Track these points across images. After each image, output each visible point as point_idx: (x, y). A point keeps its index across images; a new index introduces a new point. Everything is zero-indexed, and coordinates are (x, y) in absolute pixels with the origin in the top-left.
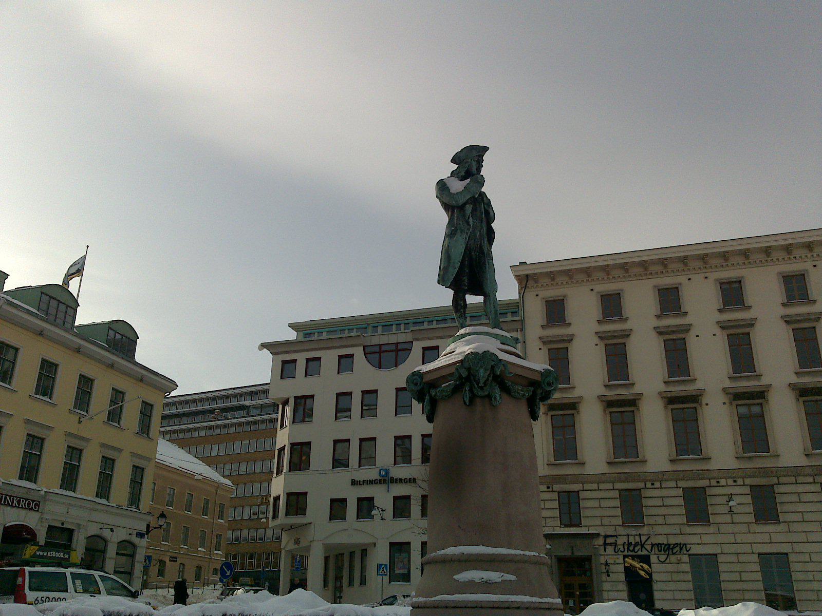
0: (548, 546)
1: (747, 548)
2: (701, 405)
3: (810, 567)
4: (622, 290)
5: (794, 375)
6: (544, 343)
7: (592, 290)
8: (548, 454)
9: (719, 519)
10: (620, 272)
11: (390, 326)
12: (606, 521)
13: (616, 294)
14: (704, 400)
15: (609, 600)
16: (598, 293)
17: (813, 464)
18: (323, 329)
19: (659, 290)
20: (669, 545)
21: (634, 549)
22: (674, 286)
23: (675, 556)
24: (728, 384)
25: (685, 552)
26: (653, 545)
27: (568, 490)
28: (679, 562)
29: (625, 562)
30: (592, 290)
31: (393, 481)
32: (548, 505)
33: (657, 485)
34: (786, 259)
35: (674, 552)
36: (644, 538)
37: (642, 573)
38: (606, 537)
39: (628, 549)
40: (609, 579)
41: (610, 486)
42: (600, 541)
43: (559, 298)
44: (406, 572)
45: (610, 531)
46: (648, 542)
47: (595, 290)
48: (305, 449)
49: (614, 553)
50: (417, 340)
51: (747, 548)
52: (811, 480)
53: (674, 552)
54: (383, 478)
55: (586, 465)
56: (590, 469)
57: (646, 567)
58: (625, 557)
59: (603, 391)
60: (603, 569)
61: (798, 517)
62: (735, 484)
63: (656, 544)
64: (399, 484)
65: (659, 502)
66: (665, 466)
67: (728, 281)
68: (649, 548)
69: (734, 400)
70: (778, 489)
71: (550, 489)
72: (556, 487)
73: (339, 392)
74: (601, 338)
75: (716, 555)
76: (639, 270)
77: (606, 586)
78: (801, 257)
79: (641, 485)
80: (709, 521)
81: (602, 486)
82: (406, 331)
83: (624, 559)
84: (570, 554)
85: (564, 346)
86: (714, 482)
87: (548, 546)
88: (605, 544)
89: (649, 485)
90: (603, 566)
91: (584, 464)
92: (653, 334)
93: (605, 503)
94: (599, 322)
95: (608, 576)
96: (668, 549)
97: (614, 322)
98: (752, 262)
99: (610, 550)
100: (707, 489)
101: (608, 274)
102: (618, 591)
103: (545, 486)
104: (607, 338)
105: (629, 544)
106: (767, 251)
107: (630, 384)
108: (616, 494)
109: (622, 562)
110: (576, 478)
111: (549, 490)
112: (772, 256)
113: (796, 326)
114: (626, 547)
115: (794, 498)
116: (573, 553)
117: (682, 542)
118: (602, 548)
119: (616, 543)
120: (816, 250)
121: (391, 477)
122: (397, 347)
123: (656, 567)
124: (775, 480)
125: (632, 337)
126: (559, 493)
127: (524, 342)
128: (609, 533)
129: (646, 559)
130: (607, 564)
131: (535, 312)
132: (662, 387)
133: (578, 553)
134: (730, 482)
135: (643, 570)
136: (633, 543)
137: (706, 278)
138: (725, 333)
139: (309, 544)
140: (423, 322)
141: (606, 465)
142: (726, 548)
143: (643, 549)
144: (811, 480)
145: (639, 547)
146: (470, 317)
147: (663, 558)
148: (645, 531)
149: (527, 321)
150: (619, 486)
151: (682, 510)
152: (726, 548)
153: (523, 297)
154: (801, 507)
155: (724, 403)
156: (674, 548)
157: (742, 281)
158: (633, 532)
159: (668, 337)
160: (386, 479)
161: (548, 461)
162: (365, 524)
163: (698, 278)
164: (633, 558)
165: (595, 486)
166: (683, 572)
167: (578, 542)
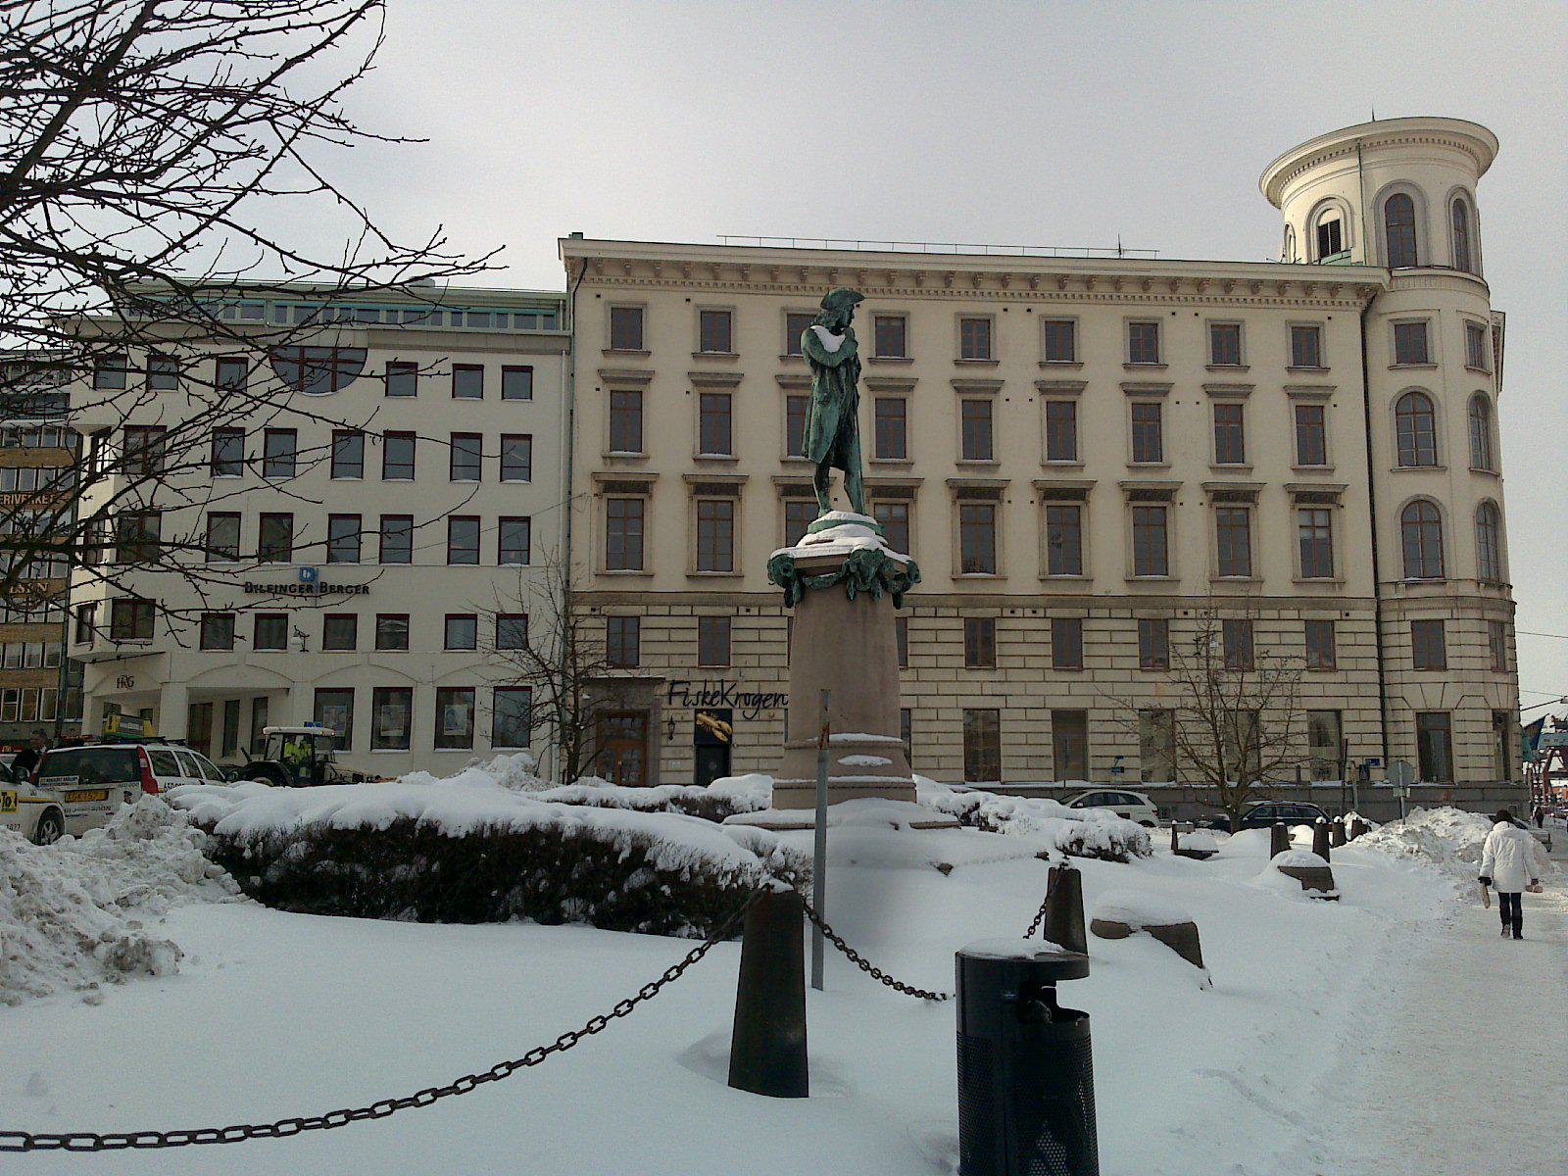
2: (1174, 504)
3: (936, 726)
4: (734, 307)
6: (605, 380)
7: (688, 300)
8: (598, 559)
9: (1008, 662)
11: (483, 316)
12: (676, 661)
13: (984, 320)
14: (1179, 497)
15: (744, 771)
18: (380, 305)
19: (789, 315)
20: (761, 696)
21: (711, 702)
23: (767, 711)
25: (781, 706)
27: (623, 615)
28: (771, 719)
29: (696, 719)
30: (688, 300)
31: (326, 589)
33: (754, 611)
34: (970, 293)
35: (766, 704)
36: (727, 686)
37: (719, 734)
38: (674, 683)
39: (703, 702)
40: (670, 742)
41: (687, 610)
42: (665, 689)
43: (635, 306)
44: (341, 733)
46: (733, 692)
48: (286, 522)
49: (682, 706)
50: (377, 346)
51: (951, 701)
52: (954, 613)
53: (766, 704)
54: (306, 584)
55: (654, 578)
57: (725, 725)
58: (697, 711)
59: (690, 468)
60: (665, 728)
61: (930, 662)
62: (1034, 615)
63: (742, 695)
65: (753, 636)
67: (887, 315)
68: (732, 699)
69: (1045, 498)
70: (645, 622)
71: (597, 613)
74: (696, 383)
75: (909, 710)
76: (763, 279)
77: (666, 753)
79: (732, 611)
81: (675, 610)
83: (696, 713)
84: (617, 708)
85: (898, 397)
88: (671, 694)
89: (742, 611)
90: (666, 725)
91: (1006, 579)
92: (774, 387)
93: (676, 636)
94: (782, 358)
95: (671, 738)
96: (759, 701)
97: (893, 362)
98: (924, 292)
99: (677, 701)
100: (1170, 622)
101: (716, 278)
105: (706, 694)
106: (948, 277)
107: (906, 464)
108: (695, 622)
109: (693, 718)
110: (1249, 602)
114: (700, 698)
115: (930, 636)
116: (622, 706)
117: (779, 692)
118: (666, 699)
121: (322, 583)
122: (335, 354)
123: (738, 727)
124: (1083, 612)
125: (653, 385)
126: (609, 617)
127: (572, 375)
129: (726, 716)
130: (671, 722)
131: (592, 324)
132: (777, 470)
134: (1028, 612)
135: (721, 729)
136: (711, 693)
137: (1029, 310)
138: (785, 393)
139: (158, 687)
140: (379, 311)
141: (685, 579)
142: (924, 702)
143: (725, 702)
144: (954, 613)
145: (719, 698)
146: (516, 314)
148: (730, 675)
149: (579, 340)
150: (700, 611)
151: (1048, 650)
152: (924, 702)
153: (574, 295)
154: (937, 649)
156: (766, 700)
157: (906, 319)
158: (716, 677)
159: (794, 392)
160: (311, 587)
161: (597, 569)
162: (269, 657)
164: (709, 713)
165: (665, 610)
166: (774, 733)
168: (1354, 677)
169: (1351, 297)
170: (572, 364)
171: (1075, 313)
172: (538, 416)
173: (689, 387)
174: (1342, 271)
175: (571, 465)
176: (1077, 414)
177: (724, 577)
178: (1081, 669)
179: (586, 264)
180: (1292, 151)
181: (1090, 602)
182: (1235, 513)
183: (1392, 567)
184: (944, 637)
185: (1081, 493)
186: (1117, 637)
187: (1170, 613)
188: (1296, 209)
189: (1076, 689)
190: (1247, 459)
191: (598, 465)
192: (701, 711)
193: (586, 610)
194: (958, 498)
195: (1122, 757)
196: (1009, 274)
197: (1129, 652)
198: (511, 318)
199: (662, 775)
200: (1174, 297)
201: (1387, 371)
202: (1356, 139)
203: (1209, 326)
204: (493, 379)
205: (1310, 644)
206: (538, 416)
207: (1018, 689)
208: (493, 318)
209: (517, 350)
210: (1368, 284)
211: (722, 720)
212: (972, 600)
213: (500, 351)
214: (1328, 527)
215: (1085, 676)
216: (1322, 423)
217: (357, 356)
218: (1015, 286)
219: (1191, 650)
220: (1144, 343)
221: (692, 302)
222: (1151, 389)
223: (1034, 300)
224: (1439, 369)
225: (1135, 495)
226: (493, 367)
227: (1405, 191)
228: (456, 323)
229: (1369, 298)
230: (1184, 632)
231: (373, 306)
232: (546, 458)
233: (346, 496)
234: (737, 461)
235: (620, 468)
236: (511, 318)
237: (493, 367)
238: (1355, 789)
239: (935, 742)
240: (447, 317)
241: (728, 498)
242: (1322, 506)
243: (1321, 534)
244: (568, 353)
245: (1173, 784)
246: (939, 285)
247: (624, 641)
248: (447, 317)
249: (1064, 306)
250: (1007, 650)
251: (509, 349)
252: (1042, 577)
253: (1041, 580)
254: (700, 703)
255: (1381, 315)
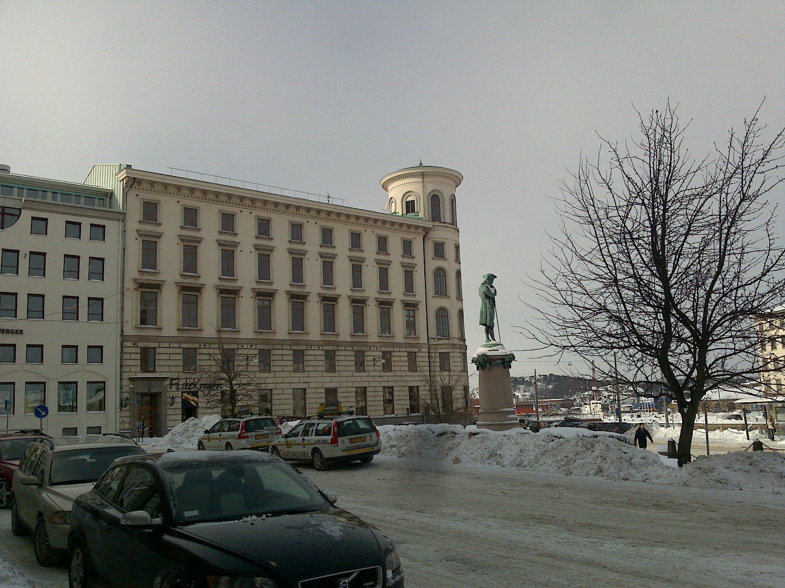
0: (131, 386)
1: (351, 384)
3: (282, 397)
5: (289, 286)
6: (140, 235)
10: (161, 188)
11: (35, 192)
12: (173, 369)
16: (183, 205)
17: (292, 339)
22: (232, 214)
24: (255, 286)
26: (201, 385)
29: (182, 396)
32: (133, 356)
33: (208, 346)
37: (193, 403)
38: (172, 379)
39: (186, 388)
40: (171, 407)
41: (178, 345)
42: (168, 382)
45: (175, 376)
46: (199, 383)
47: (181, 203)
51: (288, 386)
56: (164, 333)
57: (196, 399)
60: (169, 400)
61: (280, 369)
64: (5, 334)
66: (285, 336)
68: (198, 386)
69: (257, 296)
70: (158, 350)
71: (136, 346)
72: (141, 344)
73: (32, 251)
74: (182, 240)
77: (169, 412)
78: (236, 204)
79: (198, 346)
80: (270, 370)
82: (85, 207)
83: (182, 394)
86: (240, 347)
87: (131, 386)
88: (171, 384)
89: (202, 346)
93: (172, 357)
94: (140, 222)
97: (191, 229)
99: (174, 388)
100: (365, 352)
102: (176, 415)
103: (132, 343)
104: (381, 264)
105: (187, 384)
106: (288, 206)
108: (181, 351)
110: (156, 339)
111: (135, 346)
112: (181, 192)
113: (224, 248)
115: (280, 358)
119: (178, 384)
120: (311, 213)
124: (335, 348)
127: (125, 231)
128: (173, 377)
133: (153, 391)
134: (249, 346)
135: (194, 401)
137: (251, 213)
142: (278, 386)
144: (289, 348)
147: (206, 392)
152: (278, 386)
154: (282, 363)
155: (251, 297)
159: (224, 248)
163: (246, 211)
164: (188, 393)
165: (167, 345)
167: (153, 383)
168: (398, 374)
169: (420, 231)
170: (124, 226)
171: (387, 234)
172: (108, 249)
173: (179, 241)
174: (411, 220)
175: (124, 274)
176: (198, 252)
177: (193, 330)
178: (335, 371)
179: (134, 181)
180: (399, 171)
181: (338, 344)
182: (385, 310)
183: (433, 333)
184: (285, 358)
185: (335, 299)
186: (172, 357)
187: (365, 349)
188: (397, 191)
189: (334, 379)
190: (389, 289)
191: (136, 275)
192: (185, 392)
193: (131, 344)
194: (322, 301)
195: (352, 407)
196: (311, 208)
197: (322, 363)
198: (83, 199)
199: (168, 422)
200: (339, 220)
201: (431, 260)
202: (422, 172)
203: (290, 224)
204: (86, 230)
205: (327, 358)
206: (108, 249)
207: (313, 380)
208: (40, 193)
209: (106, 218)
210: (428, 227)
211: (194, 396)
212: (296, 343)
213: (88, 216)
214: (414, 317)
215: (337, 374)
216: (269, 262)
217: (17, 212)
218: (246, 202)
219: (372, 363)
220: (191, 217)
221: (139, 196)
222: (358, 259)
223: (245, 207)
224: (448, 261)
225: (259, 294)
226: (86, 223)
227: (440, 196)
228: (54, 199)
229: (427, 231)
230: (370, 355)
231: (12, 185)
232: (111, 270)
233: (72, 287)
234: (199, 277)
235: (146, 277)
236: (83, 199)
237: (86, 223)
238: (424, 416)
239: (282, 403)
240: (49, 195)
241: (196, 294)
242: (387, 307)
243: (411, 319)
244: (123, 221)
245: (393, 416)
246: (284, 209)
247: (147, 358)
248: (49, 195)
249: (229, 207)
250: (309, 363)
251: (95, 216)
252: (179, 328)
253: (321, 334)
254: (184, 388)
255: (430, 238)
